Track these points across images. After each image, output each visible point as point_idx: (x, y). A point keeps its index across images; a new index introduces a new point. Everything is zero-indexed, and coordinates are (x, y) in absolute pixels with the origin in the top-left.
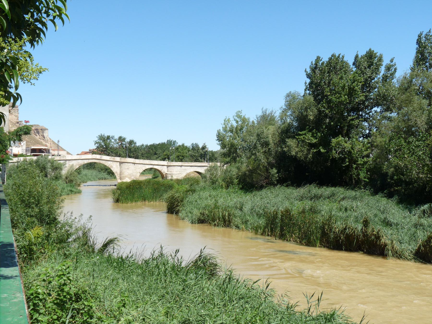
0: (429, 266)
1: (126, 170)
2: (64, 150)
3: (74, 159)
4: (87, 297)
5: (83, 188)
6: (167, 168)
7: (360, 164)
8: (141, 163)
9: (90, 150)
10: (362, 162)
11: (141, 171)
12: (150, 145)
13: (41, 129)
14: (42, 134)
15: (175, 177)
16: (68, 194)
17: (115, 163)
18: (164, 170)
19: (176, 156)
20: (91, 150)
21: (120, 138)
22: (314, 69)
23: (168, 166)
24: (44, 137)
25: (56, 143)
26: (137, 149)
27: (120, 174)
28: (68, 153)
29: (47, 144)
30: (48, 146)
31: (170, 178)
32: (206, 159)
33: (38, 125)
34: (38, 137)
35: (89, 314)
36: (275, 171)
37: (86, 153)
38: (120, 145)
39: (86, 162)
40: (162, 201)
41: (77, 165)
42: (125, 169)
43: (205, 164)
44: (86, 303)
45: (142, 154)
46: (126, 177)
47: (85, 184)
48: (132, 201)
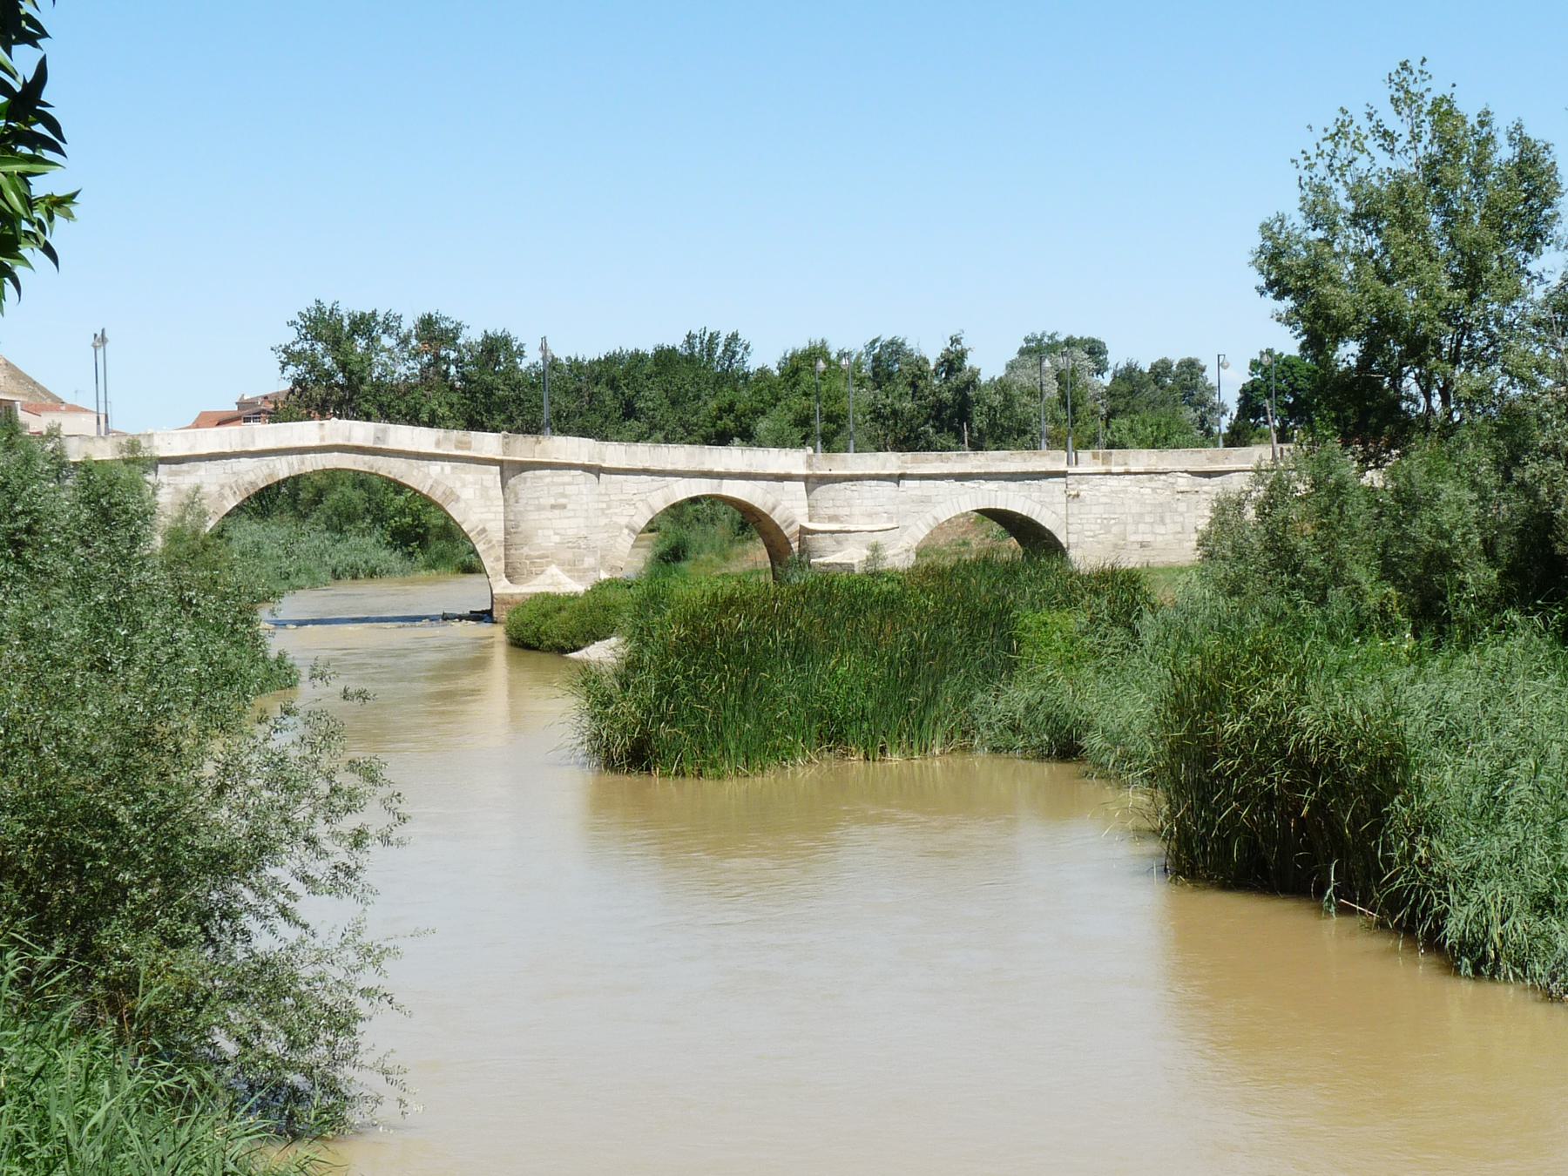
1: (548, 514)
3: (204, 451)
6: (809, 492)
8: (639, 466)
17: (472, 473)
19: (790, 416)
21: (427, 323)
23: (813, 482)
27: (507, 546)
37: (249, 412)
41: (227, 492)
42: (540, 508)
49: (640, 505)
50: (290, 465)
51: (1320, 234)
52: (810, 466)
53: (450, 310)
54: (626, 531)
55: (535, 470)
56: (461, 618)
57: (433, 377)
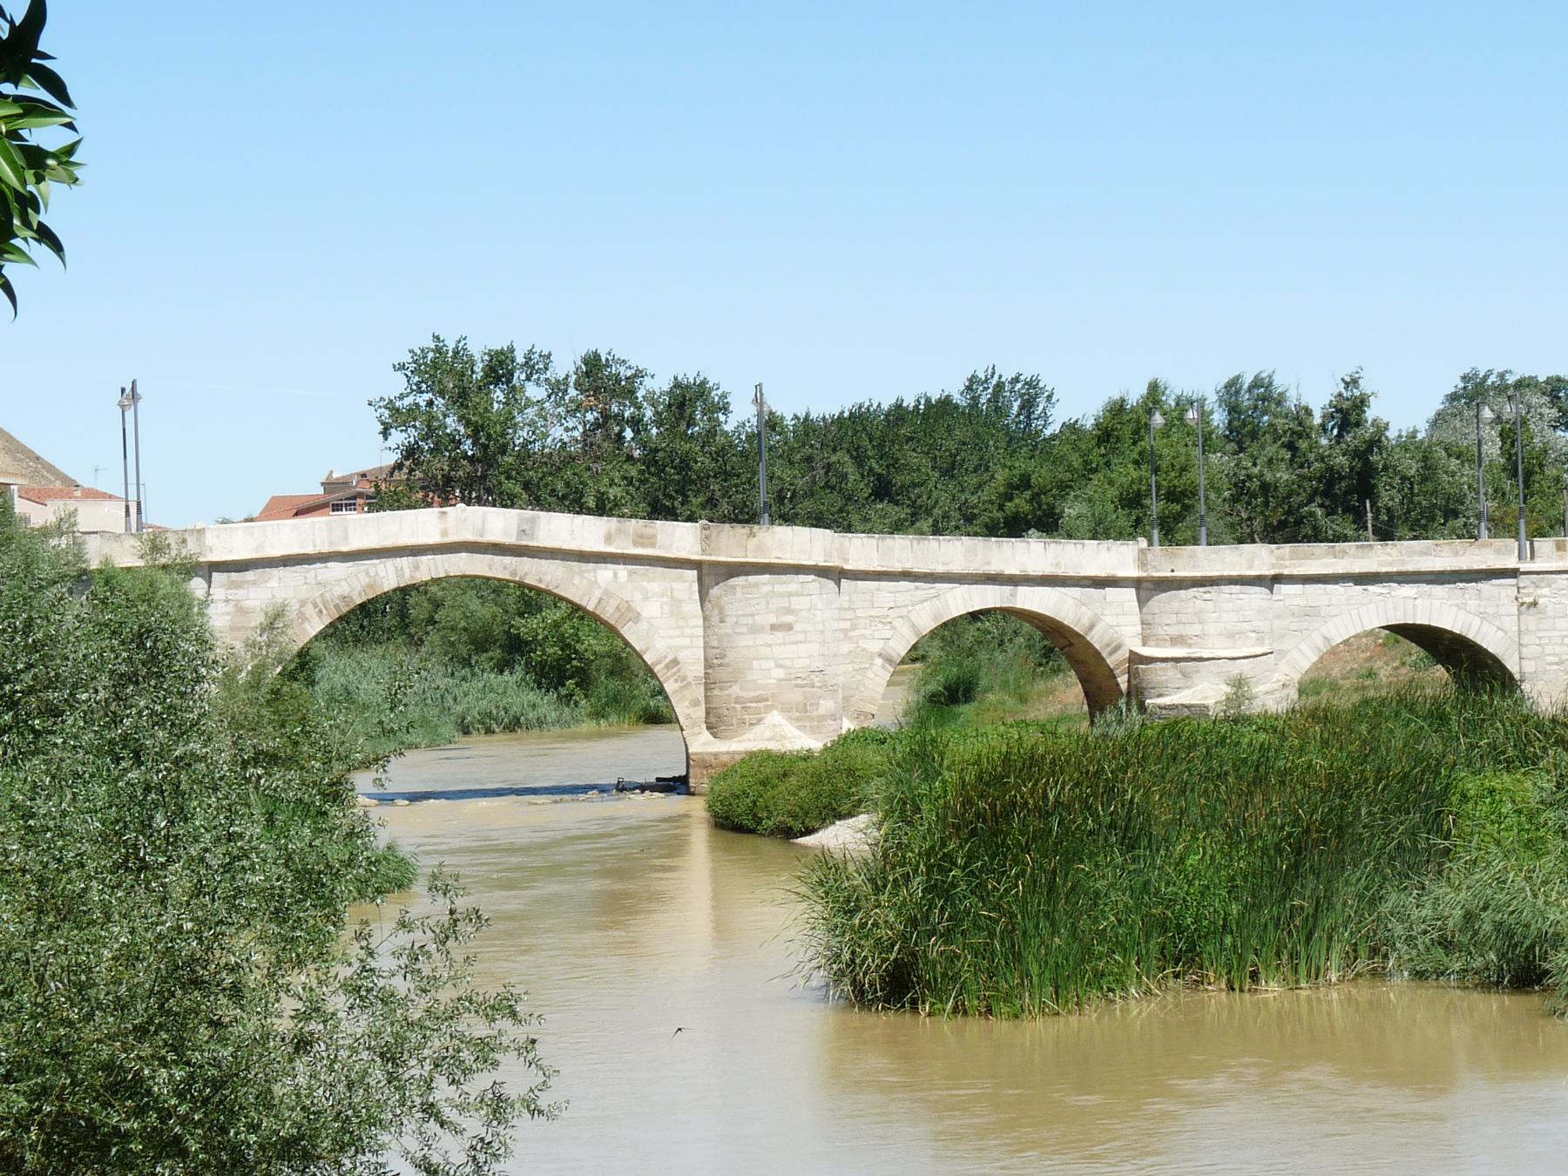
1: (767, 638)
6: (1142, 602)
8: (897, 567)
9: (329, 485)
19: (1113, 492)
21: (593, 366)
23: (1149, 588)
27: (709, 684)
38: (597, 425)
39: (389, 576)
41: (310, 611)
42: (755, 630)
46: (764, 701)
49: (898, 623)
50: (399, 571)
52: (1143, 564)
54: (879, 661)
55: (747, 574)
56: (643, 788)
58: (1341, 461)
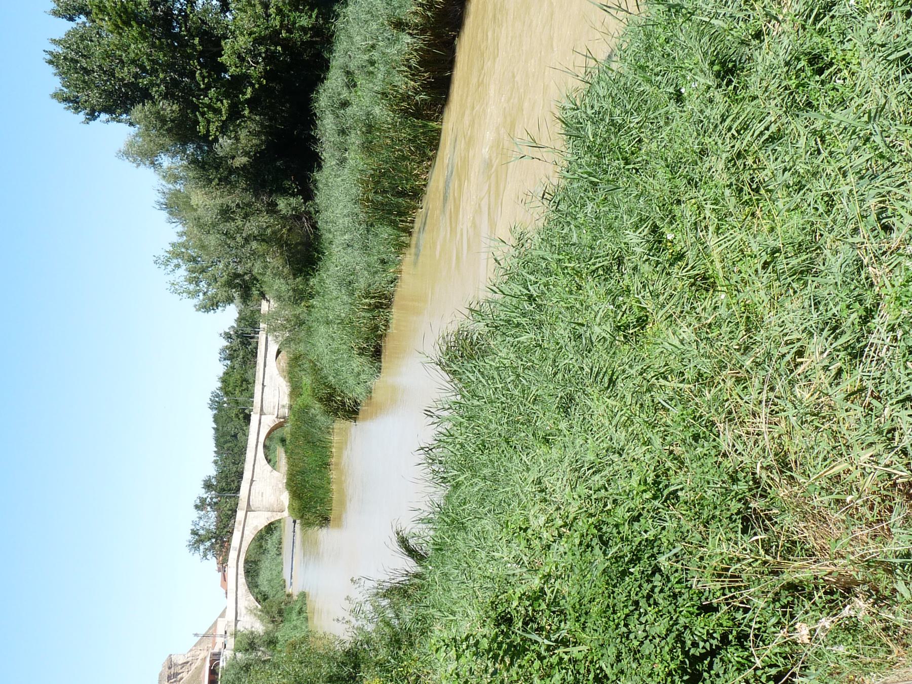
0: (473, 8)
1: (264, 498)
2: (215, 623)
4: (504, 601)
5: (294, 589)
7: (282, 22)
10: (278, 18)
11: (269, 467)
12: (217, 446)
13: (170, 668)
14: (180, 667)
15: (286, 401)
16: (307, 619)
18: (269, 421)
20: (219, 568)
22: (74, 103)
23: (262, 413)
24: (187, 663)
25: (201, 639)
26: (223, 475)
28: (223, 615)
29: (201, 657)
30: (205, 655)
31: (287, 411)
32: (252, 335)
33: (160, 675)
34: (185, 676)
35: (537, 599)
36: (282, 204)
37: (224, 578)
38: (211, 508)
39: (242, 580)
40: (333, 429)
42: (262, 500)
43: (262, 337)
44: (515, 603)
45: (234, 463)
47: (288, 583)
48: (328, 491)
51: (201, 294)
53: (193, 499)
57: (215, 506)
58: (239, 340)
